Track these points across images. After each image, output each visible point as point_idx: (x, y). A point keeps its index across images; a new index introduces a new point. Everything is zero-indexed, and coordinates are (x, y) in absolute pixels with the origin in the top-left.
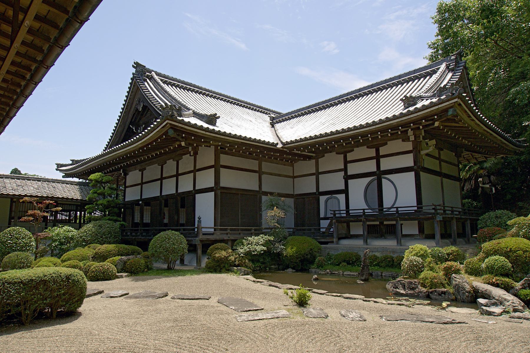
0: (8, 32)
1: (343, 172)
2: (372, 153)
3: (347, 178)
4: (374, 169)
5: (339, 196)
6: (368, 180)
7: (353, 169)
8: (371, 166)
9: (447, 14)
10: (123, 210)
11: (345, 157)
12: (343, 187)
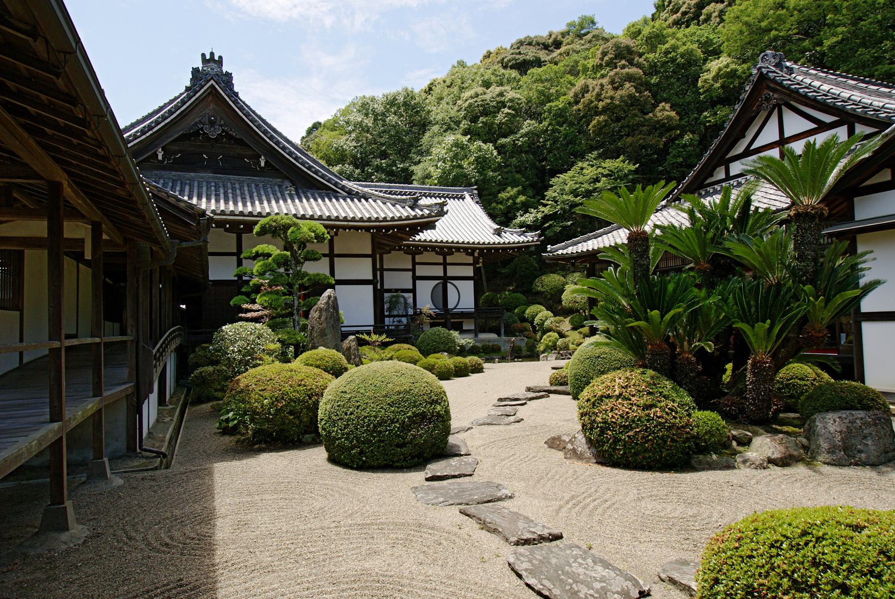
0: (802, 379)
1: (411, 273)
2: (440, 259)
3: (415, 278)
4: (442, 274)
5: (406, 295)
7: (421, 271)
8: (438, 271)
10: (184, 307)
11: (413, 259)
12: (411, 287)
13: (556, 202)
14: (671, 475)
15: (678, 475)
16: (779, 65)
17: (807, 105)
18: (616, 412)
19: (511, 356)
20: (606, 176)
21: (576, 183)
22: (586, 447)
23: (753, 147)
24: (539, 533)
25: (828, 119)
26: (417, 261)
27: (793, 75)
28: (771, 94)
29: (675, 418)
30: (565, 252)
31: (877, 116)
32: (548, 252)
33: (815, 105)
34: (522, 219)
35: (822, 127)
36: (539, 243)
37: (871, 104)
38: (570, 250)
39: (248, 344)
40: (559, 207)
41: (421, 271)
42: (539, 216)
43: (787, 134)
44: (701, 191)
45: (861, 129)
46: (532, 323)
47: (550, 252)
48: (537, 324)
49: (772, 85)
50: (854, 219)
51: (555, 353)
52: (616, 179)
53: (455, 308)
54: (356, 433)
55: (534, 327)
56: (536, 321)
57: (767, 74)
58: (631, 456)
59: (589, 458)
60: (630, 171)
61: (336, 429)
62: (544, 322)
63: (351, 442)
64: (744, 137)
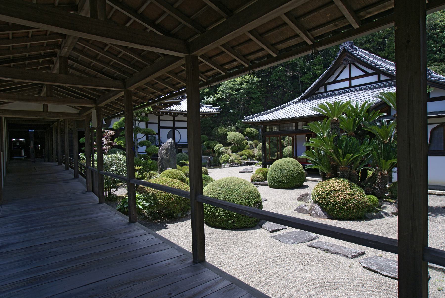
2: (172, 118)
3: (160, 128)
4: (172, 126)
6: (170, 129)
8: (171, 124)
9: (372, 209)
10: (13, 140)
11: (159, 118)
13: (223, 93)
14: (364, 222)
15: (367, 222)
16: (351, 47)
17: (363, 65)
18: (340, 197)
19: (209, 165)
20: (246, 82)
21: (232, 85)
22: (321, 212)
23: (337, 79)
24: (357, 252)
25: (370, 71)
26: (161, 119)
27: (358, 52)
28: (348, 58)
29: (363, 199)
30: (254, 120)
31: (392, 73)
32: (244, 119)
33: (363, 63)
34: (207, 100)
35: (367, 75)
36: (219, 112)
37: (389, 68)
38: (256, 119)
39: (120, 166)
40: (224, 95)
41: (163, 124)
42: (215, 99)
43: (352, 76)
44: (313, 96)
45: (383, 78)
46: (213, 149)
47: (246, 119)
48: (216, 150)
49: (349, 55)
50: (391, 115)
51: (228, 164)
52: (251, 84)
53: (178, 142)
54: (231, 213)
55: (214, 151)
56: (215, 148)
57: (347, 50)
58: (346, 215)
59: (324, 217)
60: (257, 81)
61: (218, 211)
62: (219, 149)
63: (228, 217)
64: (333, 75)
